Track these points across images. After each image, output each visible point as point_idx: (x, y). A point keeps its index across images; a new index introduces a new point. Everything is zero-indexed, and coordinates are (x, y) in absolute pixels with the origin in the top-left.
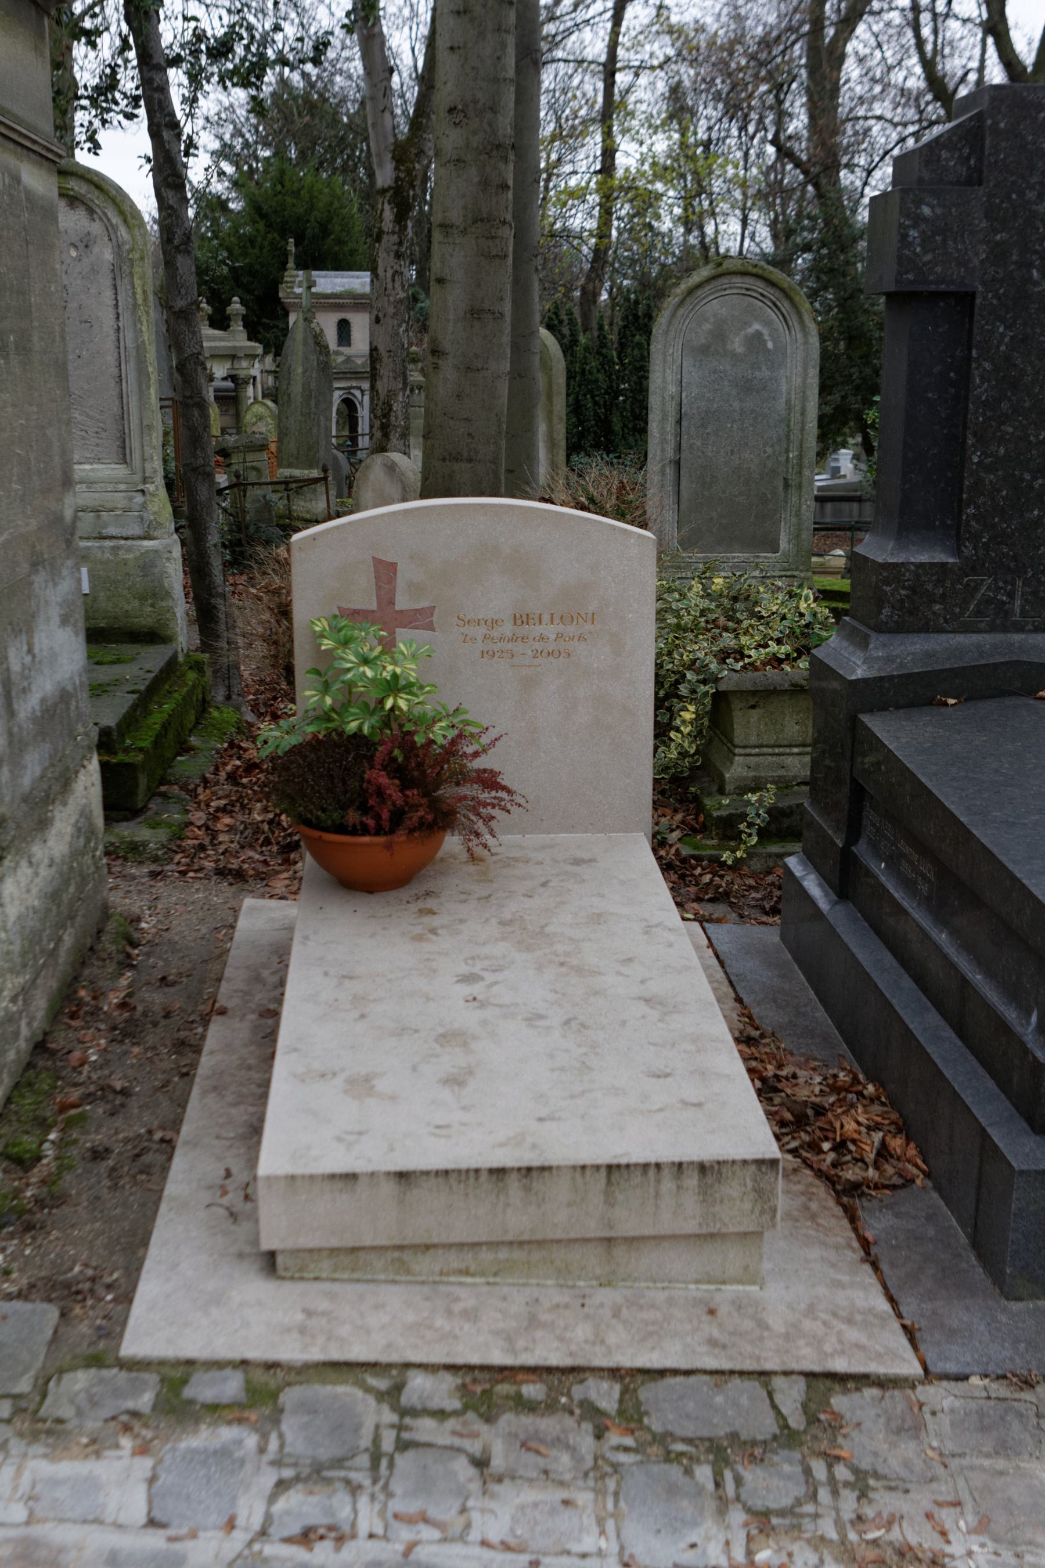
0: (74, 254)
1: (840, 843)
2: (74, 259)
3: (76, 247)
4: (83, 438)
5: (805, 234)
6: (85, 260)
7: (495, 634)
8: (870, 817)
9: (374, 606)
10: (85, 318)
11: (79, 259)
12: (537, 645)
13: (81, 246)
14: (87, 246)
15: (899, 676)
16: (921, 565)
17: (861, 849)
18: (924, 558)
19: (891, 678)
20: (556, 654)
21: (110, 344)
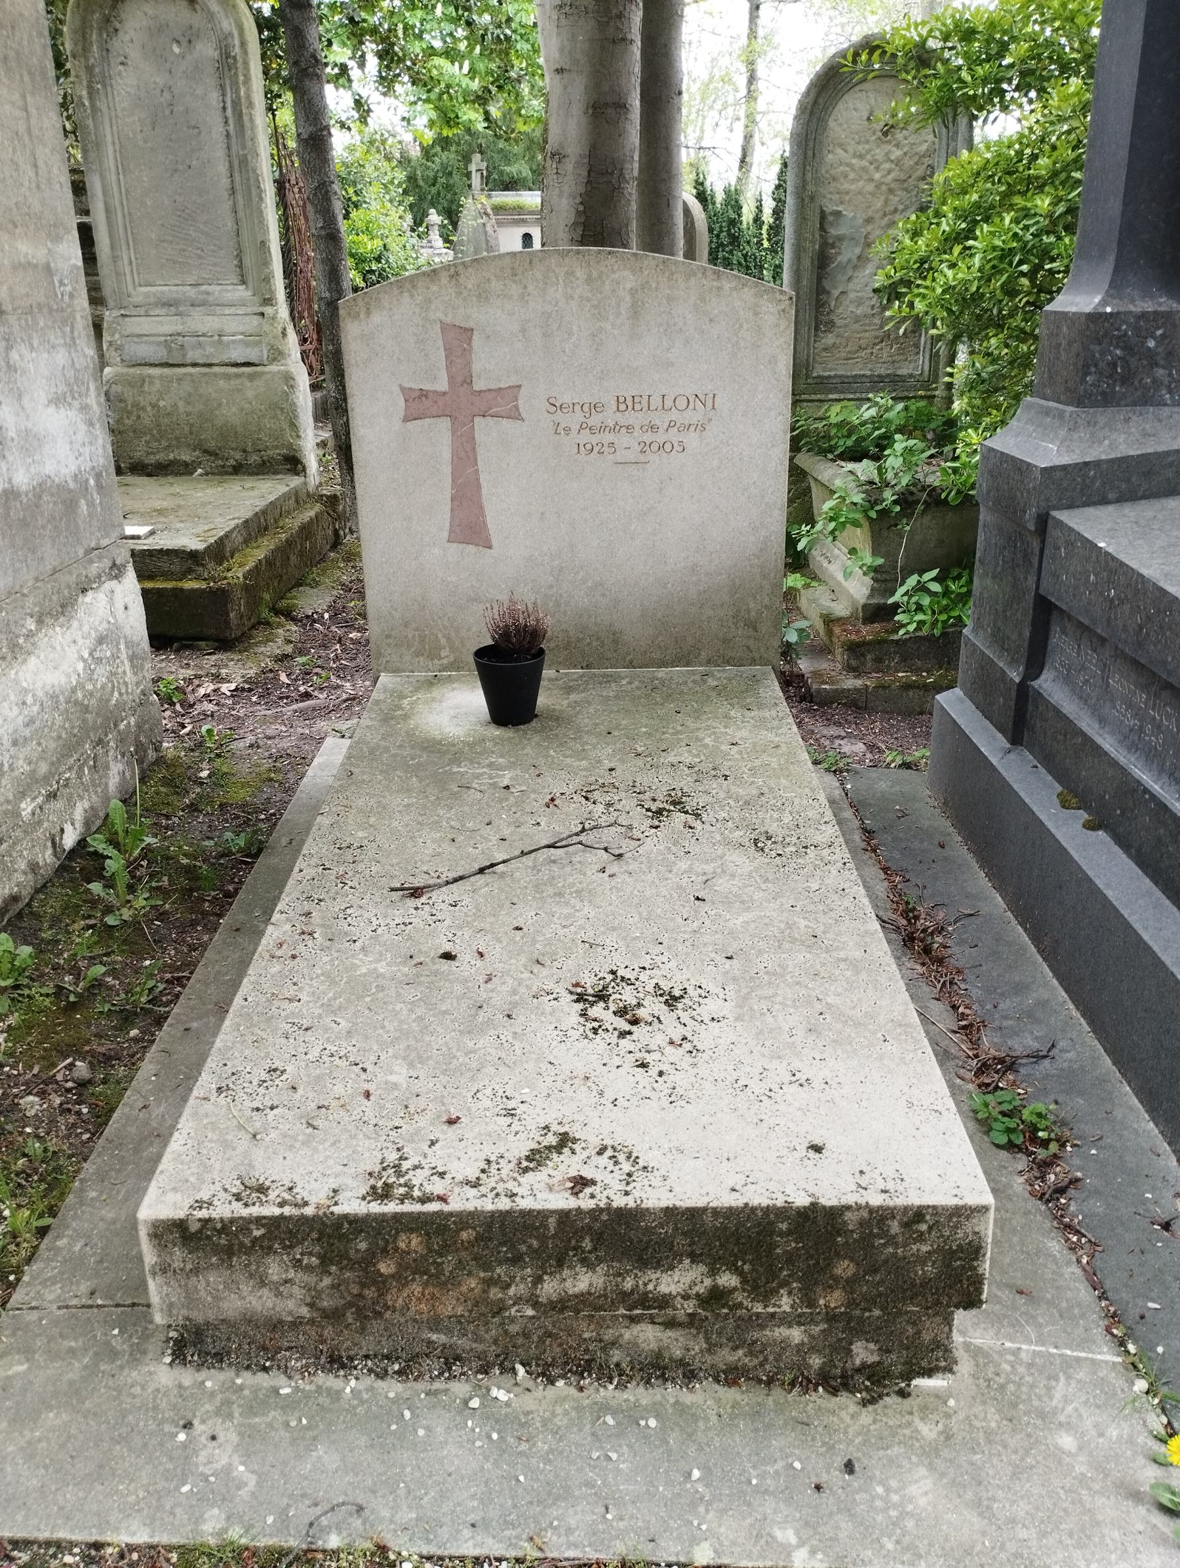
0: (176, 50)
1: (1015, 676)
2: (177, 56)
3: (178, 42)
4: (200, 257)
5: (611, 694)
6: (189, 57)
7: (595, 420)
8: (1060, 641)
9: (442, 385)
10: (193, 123)
11: (183, 56)
12: (648, 437)
13: (184, 41)
14: (190, 41)
15: (1112, 461)
16: (1143, 315)
17: (1048, 684)
18: (1148, 306)
19: (1097, 464)
20: (668, 447)
21: (220, 153)
